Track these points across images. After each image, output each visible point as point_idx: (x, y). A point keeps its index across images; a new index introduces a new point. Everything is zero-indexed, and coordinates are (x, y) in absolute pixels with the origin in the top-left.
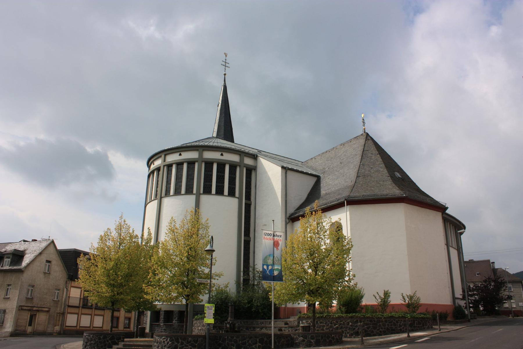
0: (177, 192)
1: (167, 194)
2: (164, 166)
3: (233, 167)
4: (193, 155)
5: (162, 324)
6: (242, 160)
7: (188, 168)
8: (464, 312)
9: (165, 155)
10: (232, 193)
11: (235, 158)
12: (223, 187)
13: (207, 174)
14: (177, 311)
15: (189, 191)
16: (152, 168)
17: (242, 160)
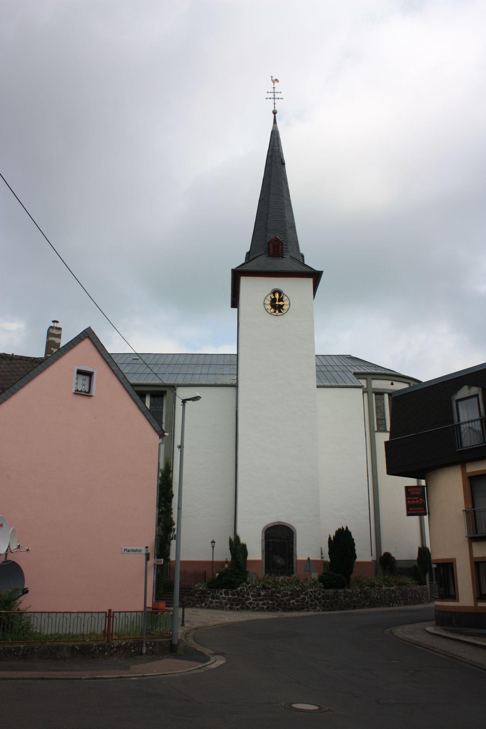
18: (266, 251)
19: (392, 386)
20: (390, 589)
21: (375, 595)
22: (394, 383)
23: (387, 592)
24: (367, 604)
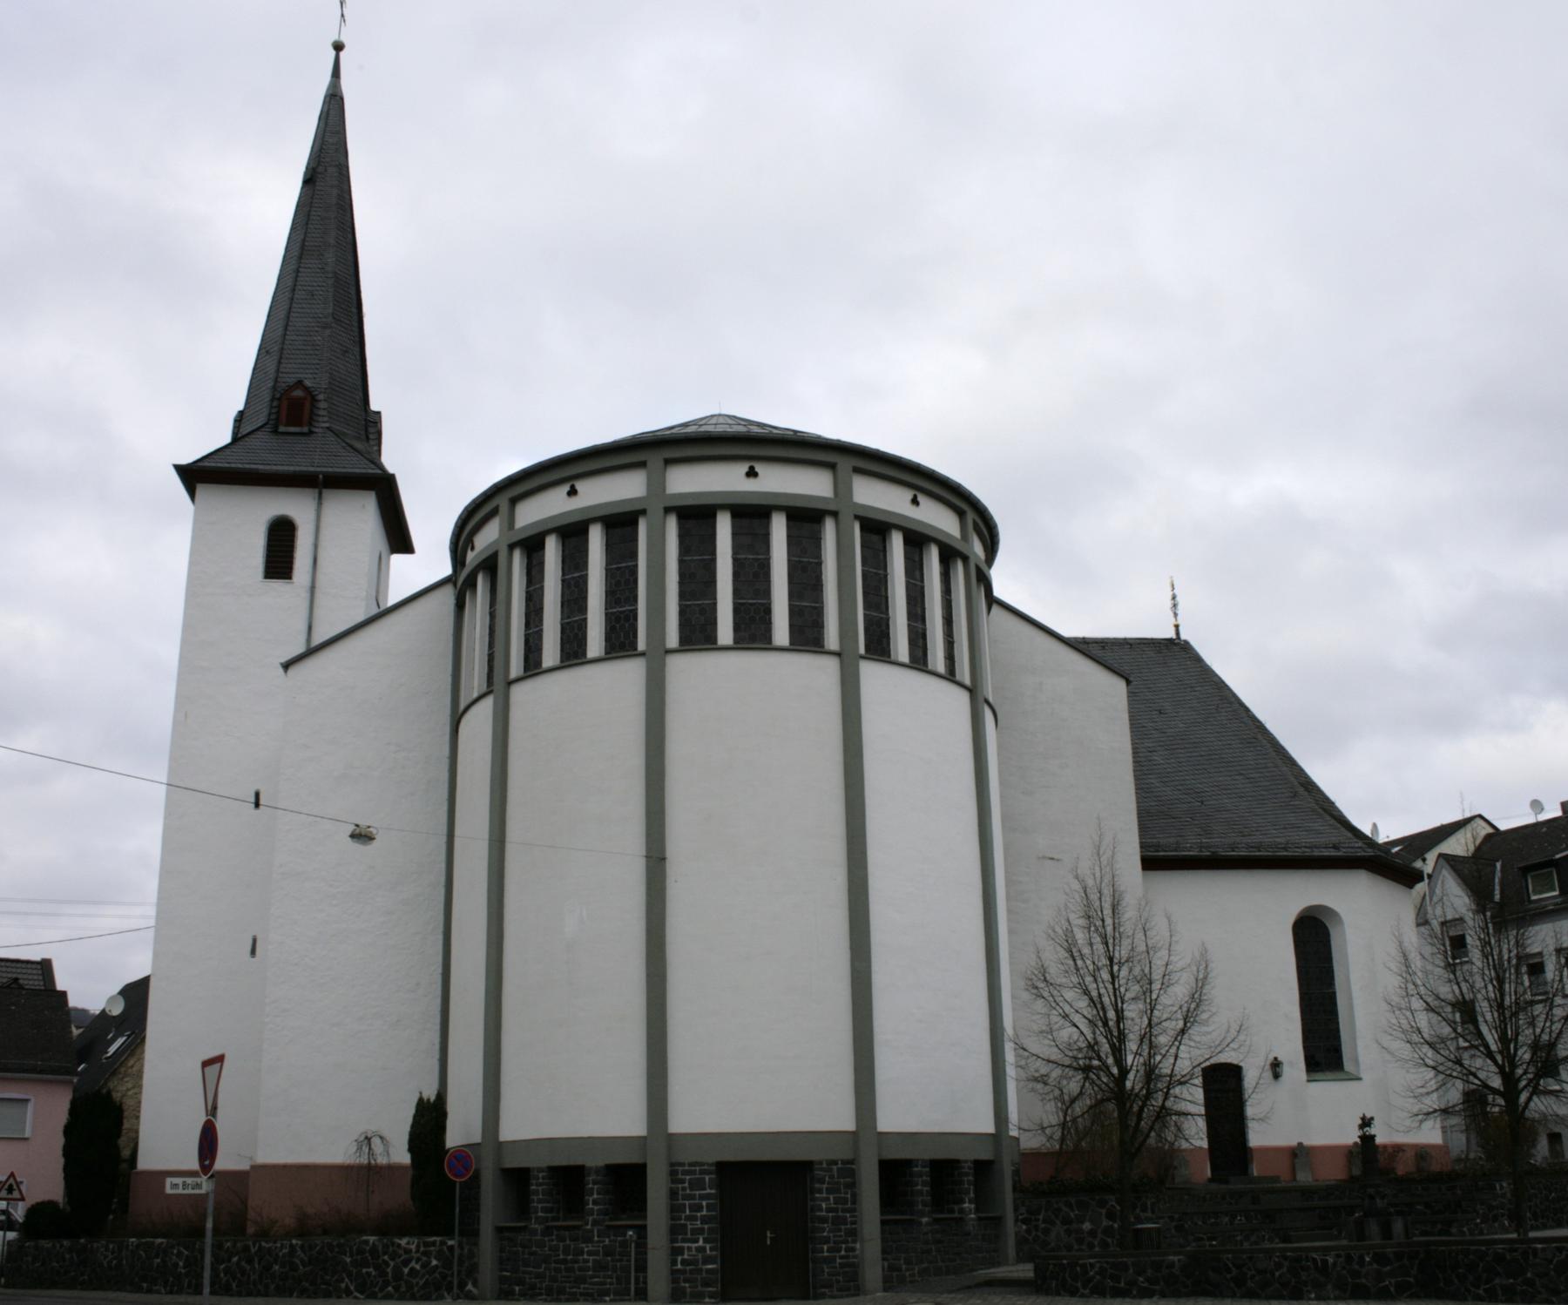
0: (574, 652)
1: (533, 665)
2: (512, 547)
3: (805, 518)
4: (623, 488)
5: (925, 1220)
6: (841, 489)
7: (610, 547)
8: (1534, 1143)
9: (514, 501)
10: (807, 636)
11: (810, 484)
12: (713, 607)
13: (876, 574)
14: (971, 1161)
15: (621, 642)
16: (472, 560)
17: (841, 489)
18: (271, 422)
19: (752, 480)
20: (153, 1243)
21: (106, 1257)
22: (759, 468)
23: (142, 1253)
24: (81, 1279)
